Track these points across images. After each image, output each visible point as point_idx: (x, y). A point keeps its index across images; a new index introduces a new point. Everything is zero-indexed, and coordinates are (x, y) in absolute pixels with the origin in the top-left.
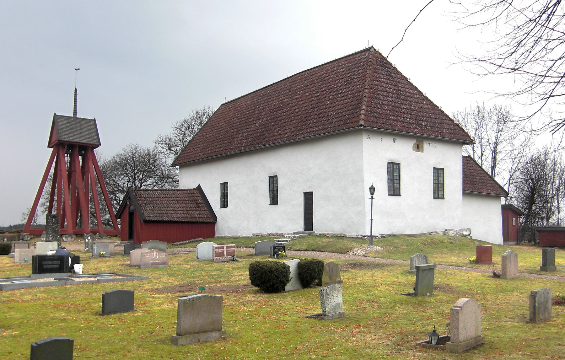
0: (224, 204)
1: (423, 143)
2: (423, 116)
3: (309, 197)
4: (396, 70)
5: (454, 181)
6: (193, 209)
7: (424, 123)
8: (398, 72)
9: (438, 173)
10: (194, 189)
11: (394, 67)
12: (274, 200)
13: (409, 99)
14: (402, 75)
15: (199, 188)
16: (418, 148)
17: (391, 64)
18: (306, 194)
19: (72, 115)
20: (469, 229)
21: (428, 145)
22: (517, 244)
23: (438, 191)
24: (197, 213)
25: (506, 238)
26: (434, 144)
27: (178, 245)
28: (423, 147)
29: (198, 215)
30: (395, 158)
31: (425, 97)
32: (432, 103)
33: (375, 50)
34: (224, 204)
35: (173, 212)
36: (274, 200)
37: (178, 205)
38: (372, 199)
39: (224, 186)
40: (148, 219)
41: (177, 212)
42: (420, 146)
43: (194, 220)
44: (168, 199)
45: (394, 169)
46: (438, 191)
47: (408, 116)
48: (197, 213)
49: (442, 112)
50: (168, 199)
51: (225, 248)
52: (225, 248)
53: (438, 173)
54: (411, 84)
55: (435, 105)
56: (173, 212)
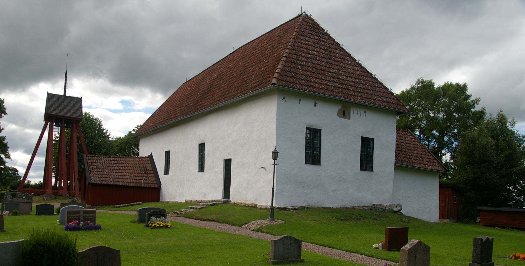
0: (167, 172)
1: (350, 110)
2: (352, 82)
3: (228, 163)
4: (329, 35)
5: (385, 154)
6: (140, 175)
7: (353, 88)
8: (331, 38)
9: (367, 144)
10: (146, 157)
11: (327, 33)
12: (201, 168)
13: (339, 64)
14: (334, 41)
15: (151, 157)
16: (344, 114)
17: (323, 30)
18: (166, 152)
19: (62, 94)
20: (400, 206)
21: (356, 112)
22: (456, 222)
23: (367, 162)
24: (143, 178)
25: (443, 214)
26: (363, 112)
27: (117, 207)
28: (349, 114)
29: (143, 181)
30: (316, 124)
31: (375, 78)
32: (365, 69)
33: (307, 15)
34: (167, 172)
35: (120, 177)
36: (201, 168)
37: (127, 171)
38: (274, 164)
39: (168, 154)
40: (93, 182)
41: (124, 177)
42: (346, 113)
43: (139, 185)
44: (119, 165)
45: (313, 137)
46: (367, 162)
47: (335, 80)
48: (143, 178)
49: (376, 79)
50: (119, 165)
51: (82, 213)
52: (82, 213)
53: (367, 144)
54: (344, 51)
55: (368, 72)
56: (120, 177)
